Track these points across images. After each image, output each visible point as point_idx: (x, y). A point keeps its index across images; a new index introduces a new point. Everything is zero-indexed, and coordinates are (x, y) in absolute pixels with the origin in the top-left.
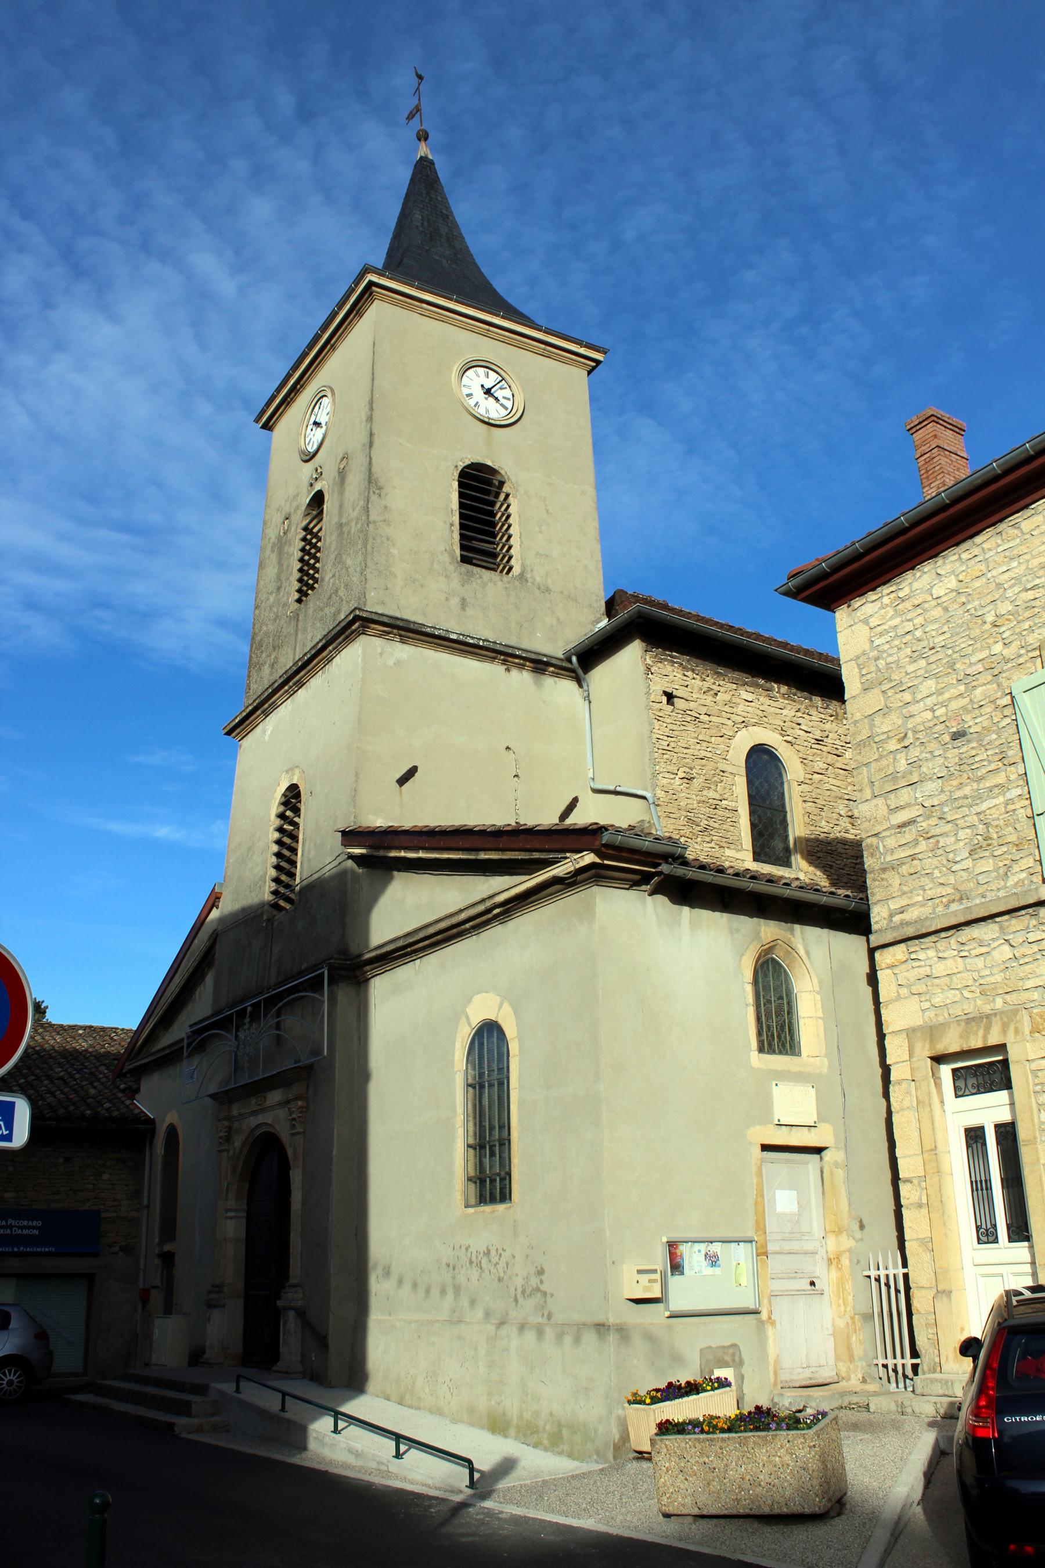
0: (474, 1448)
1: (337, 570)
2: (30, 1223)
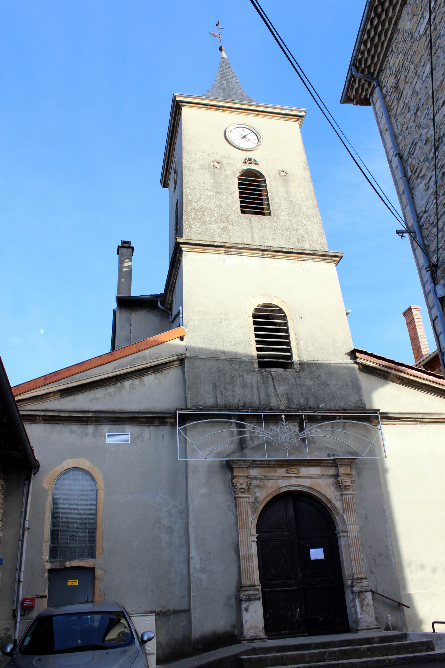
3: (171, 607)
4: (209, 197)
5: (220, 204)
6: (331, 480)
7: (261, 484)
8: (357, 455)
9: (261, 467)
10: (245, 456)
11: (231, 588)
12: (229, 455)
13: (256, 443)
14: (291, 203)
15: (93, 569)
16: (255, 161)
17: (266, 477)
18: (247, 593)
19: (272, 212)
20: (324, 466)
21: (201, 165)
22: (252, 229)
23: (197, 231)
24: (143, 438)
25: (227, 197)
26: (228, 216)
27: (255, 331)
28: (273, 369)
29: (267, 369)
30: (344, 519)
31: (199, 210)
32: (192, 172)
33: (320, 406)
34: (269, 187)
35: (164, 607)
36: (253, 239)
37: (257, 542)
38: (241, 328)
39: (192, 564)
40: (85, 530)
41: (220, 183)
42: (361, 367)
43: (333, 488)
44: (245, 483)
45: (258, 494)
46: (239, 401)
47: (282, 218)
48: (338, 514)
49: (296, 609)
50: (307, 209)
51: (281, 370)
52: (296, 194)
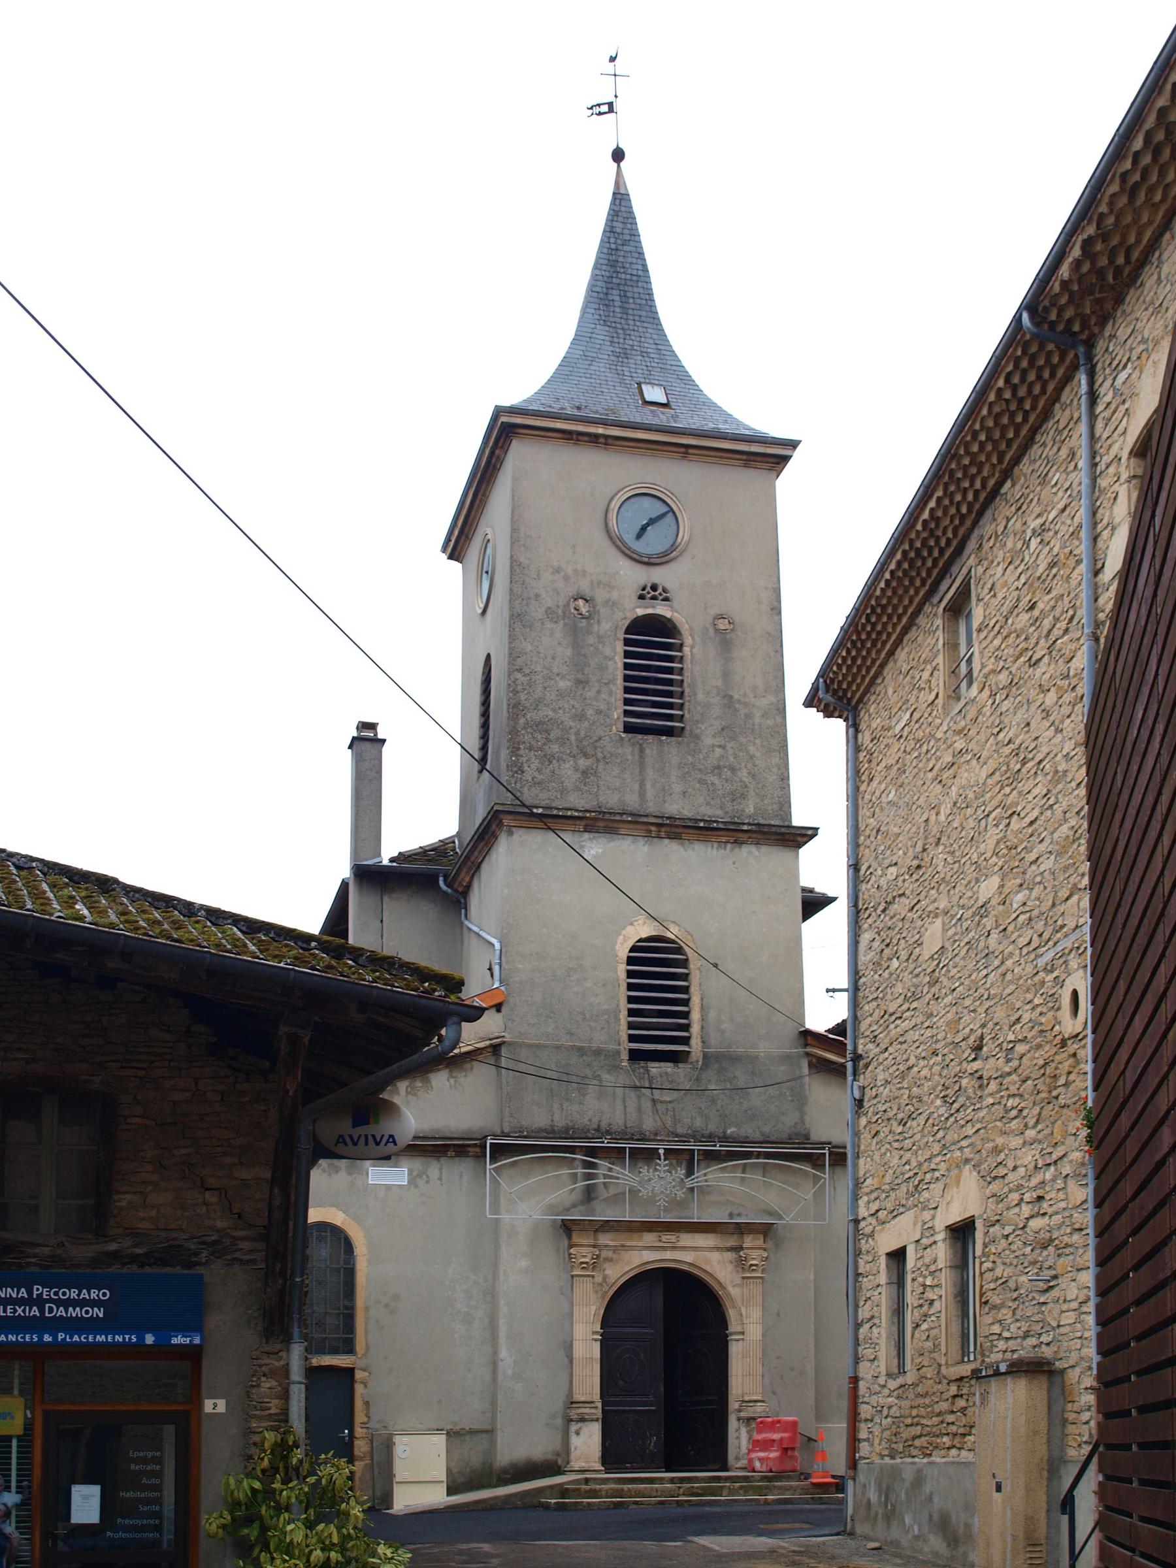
0: (386, 1358)
1: (1016, 1142)
2: (84, 1294)
3: (466, 1424)
4: (561, 694)
5: (583, 710)
6: (729, 1255)
7: (615, 1256)
8: (781, 1218)
9: (617, 1231)
10: (592, 1213)
11: (559, 1405)
12: (567, 1210)
13: (612, 1191)
14: (729, 701)
15: (350, 1372)
16: (665, 590)
17: (623, 1246)
18: (580, 1411)
19: (687, 704)
20: (721, 1233)
21: (549, 608)
22: (642, 765)
23: (533, 779)
24: (428, 1177)
25: (599, 692)
26: (596, 741)
27: (628, 977)
28: (651, 1064)
29: (642, 1063)
30: (741, 1315)
31: (540, 726)
32: (528, 630)
33: (729, 1132)
34: (689, 661)
35: (456, 1425)
36: (642, 794)
37: (601, 1341)
38: (604, 985)
39: (500, 1368)
40: (339, 1314)
41: (585, 656)
42: (814, 1060)
43: (730, 1268)
44: (590, 1256)
45: (608, 1272)
46: (590, 1120)
47: (708, 741)
48: (734, 1307)
49: (651, 1436)
50: (763, 716)
51: (668, 1067)
52: (744, 677)
